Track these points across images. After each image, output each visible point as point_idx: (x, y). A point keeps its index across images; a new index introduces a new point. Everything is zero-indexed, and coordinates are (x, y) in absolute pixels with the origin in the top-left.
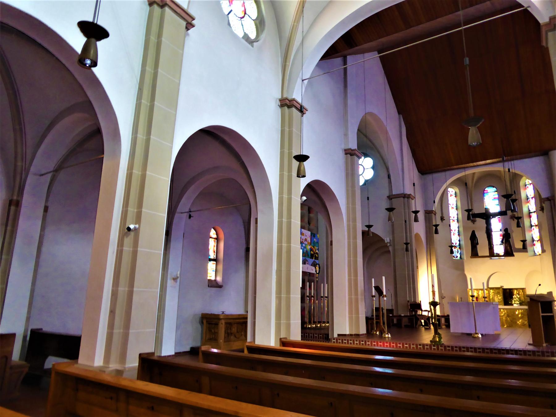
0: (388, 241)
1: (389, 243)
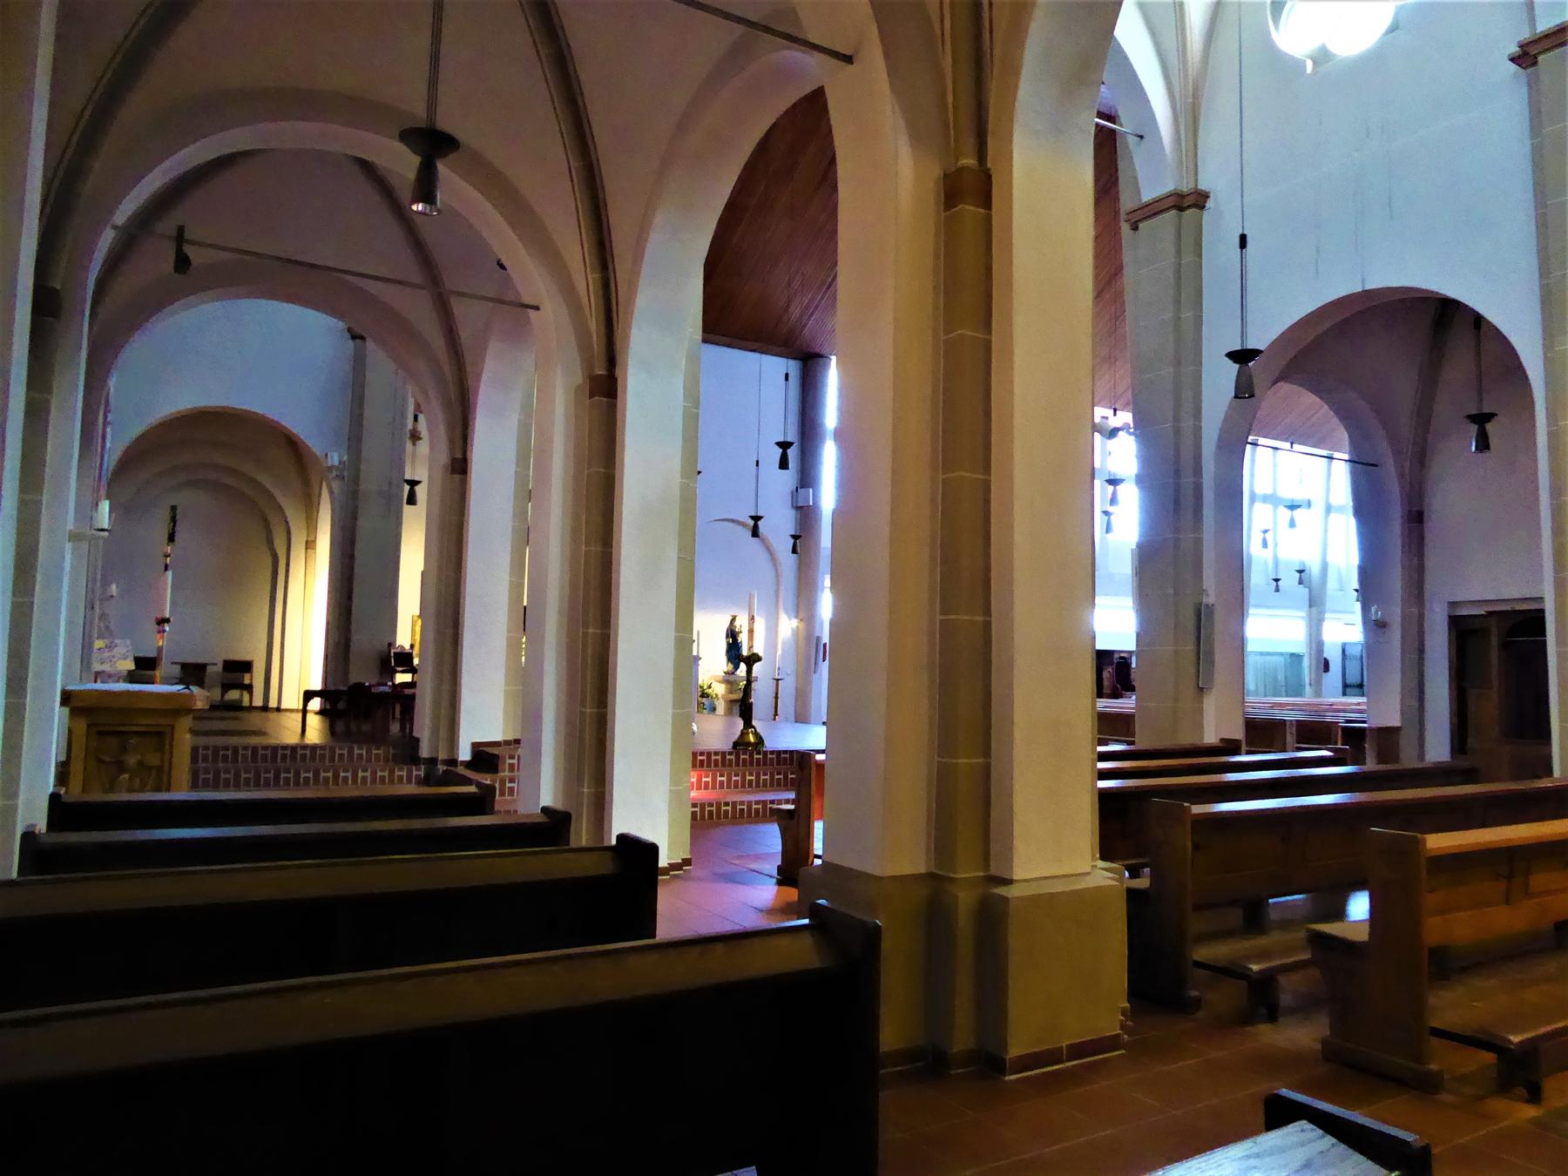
0: (336, 463)
1: (337, 468)
